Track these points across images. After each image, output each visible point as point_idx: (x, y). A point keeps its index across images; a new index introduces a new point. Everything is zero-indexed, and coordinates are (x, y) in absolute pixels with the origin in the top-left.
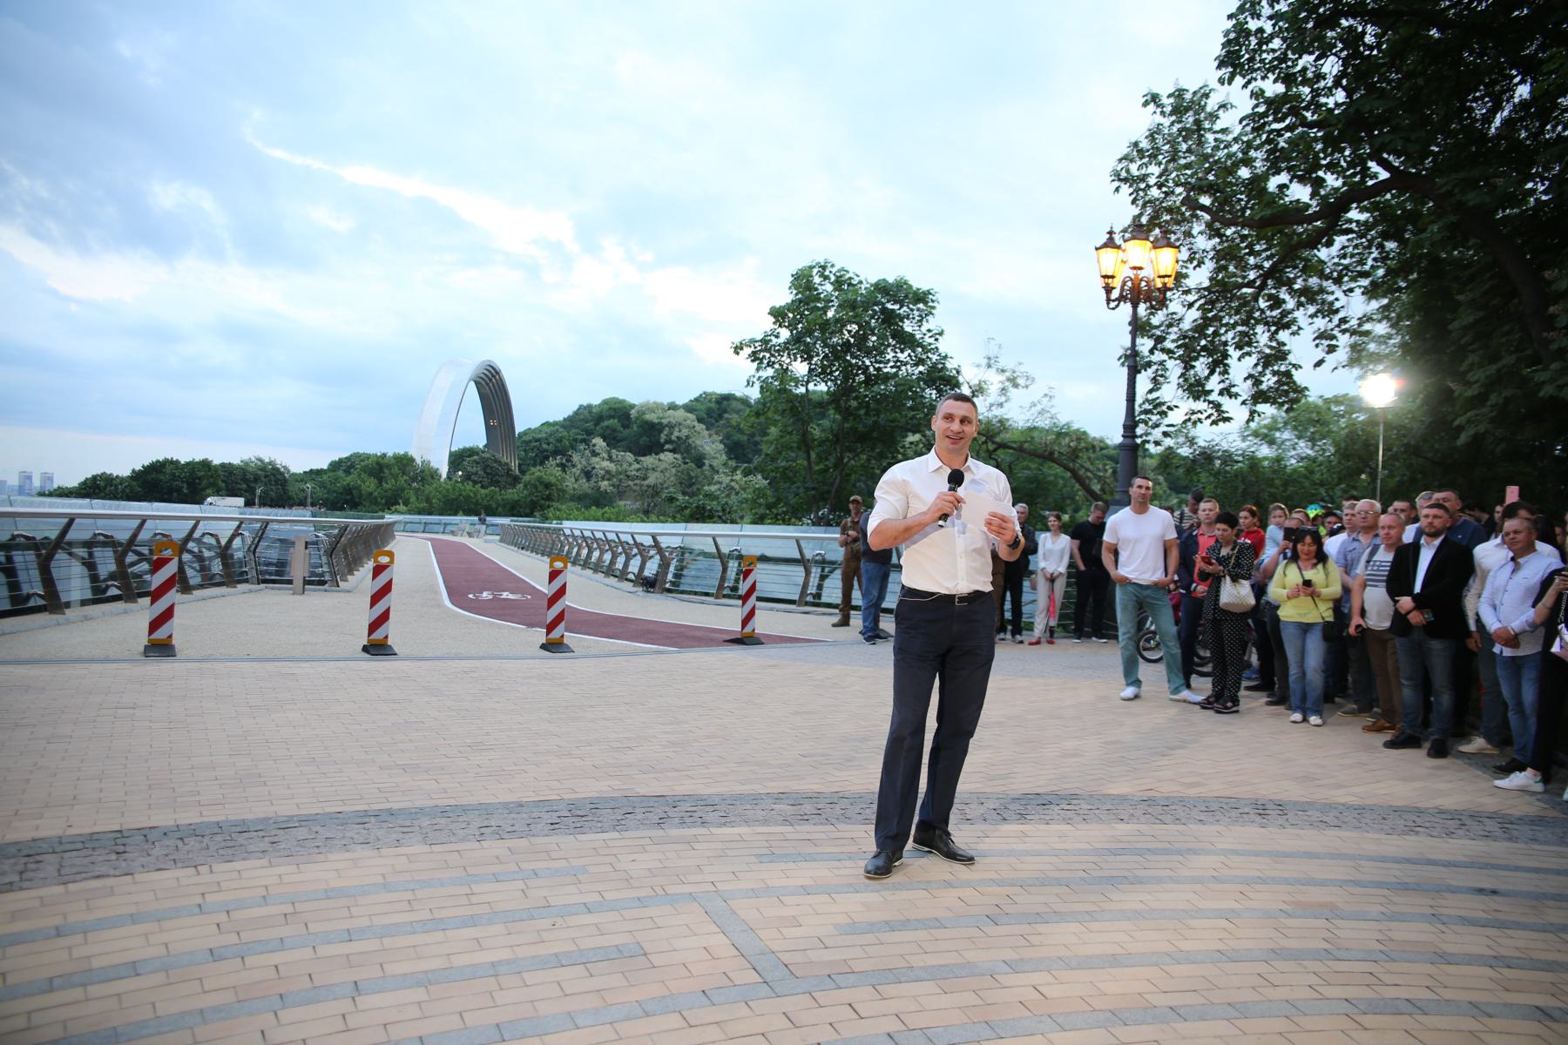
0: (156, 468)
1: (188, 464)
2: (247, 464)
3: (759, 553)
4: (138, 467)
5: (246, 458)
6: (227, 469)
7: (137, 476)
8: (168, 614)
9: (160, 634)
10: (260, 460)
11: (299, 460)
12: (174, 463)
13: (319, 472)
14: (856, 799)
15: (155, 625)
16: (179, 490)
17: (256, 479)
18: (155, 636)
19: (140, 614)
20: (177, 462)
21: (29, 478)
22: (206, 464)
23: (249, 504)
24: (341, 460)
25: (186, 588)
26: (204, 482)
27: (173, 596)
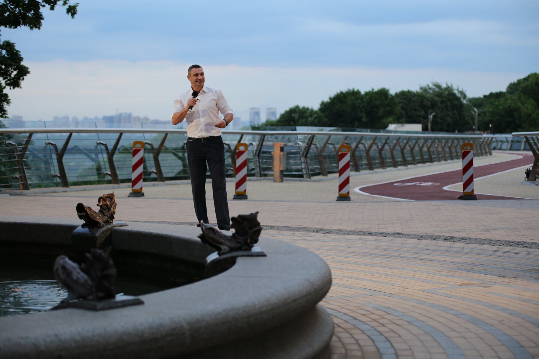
0: (341, 99)
1: (367, 94)
2: (425, 90)
3: (281, 109)
4: (326, 99)
5: (424, 84)
6: (405, 96)
7: (325, 107)
8: (346, 182)
9: (344, 191)
10: (438, 86)
11: (475, 85)
12: (355, 94)
13: (499, 95)
14: (475, 178)
15: (341, 187)
16: (359, 119)
17: (433, 105)
18: (341, 192)
19: (335, 180)
20: (358, 92)
21: (257, 114)
22: (383, 93)
23: (425, 129)
24: (519, 82)
25: (357, 169)
26: (381, 111)
27: (348, 173)
